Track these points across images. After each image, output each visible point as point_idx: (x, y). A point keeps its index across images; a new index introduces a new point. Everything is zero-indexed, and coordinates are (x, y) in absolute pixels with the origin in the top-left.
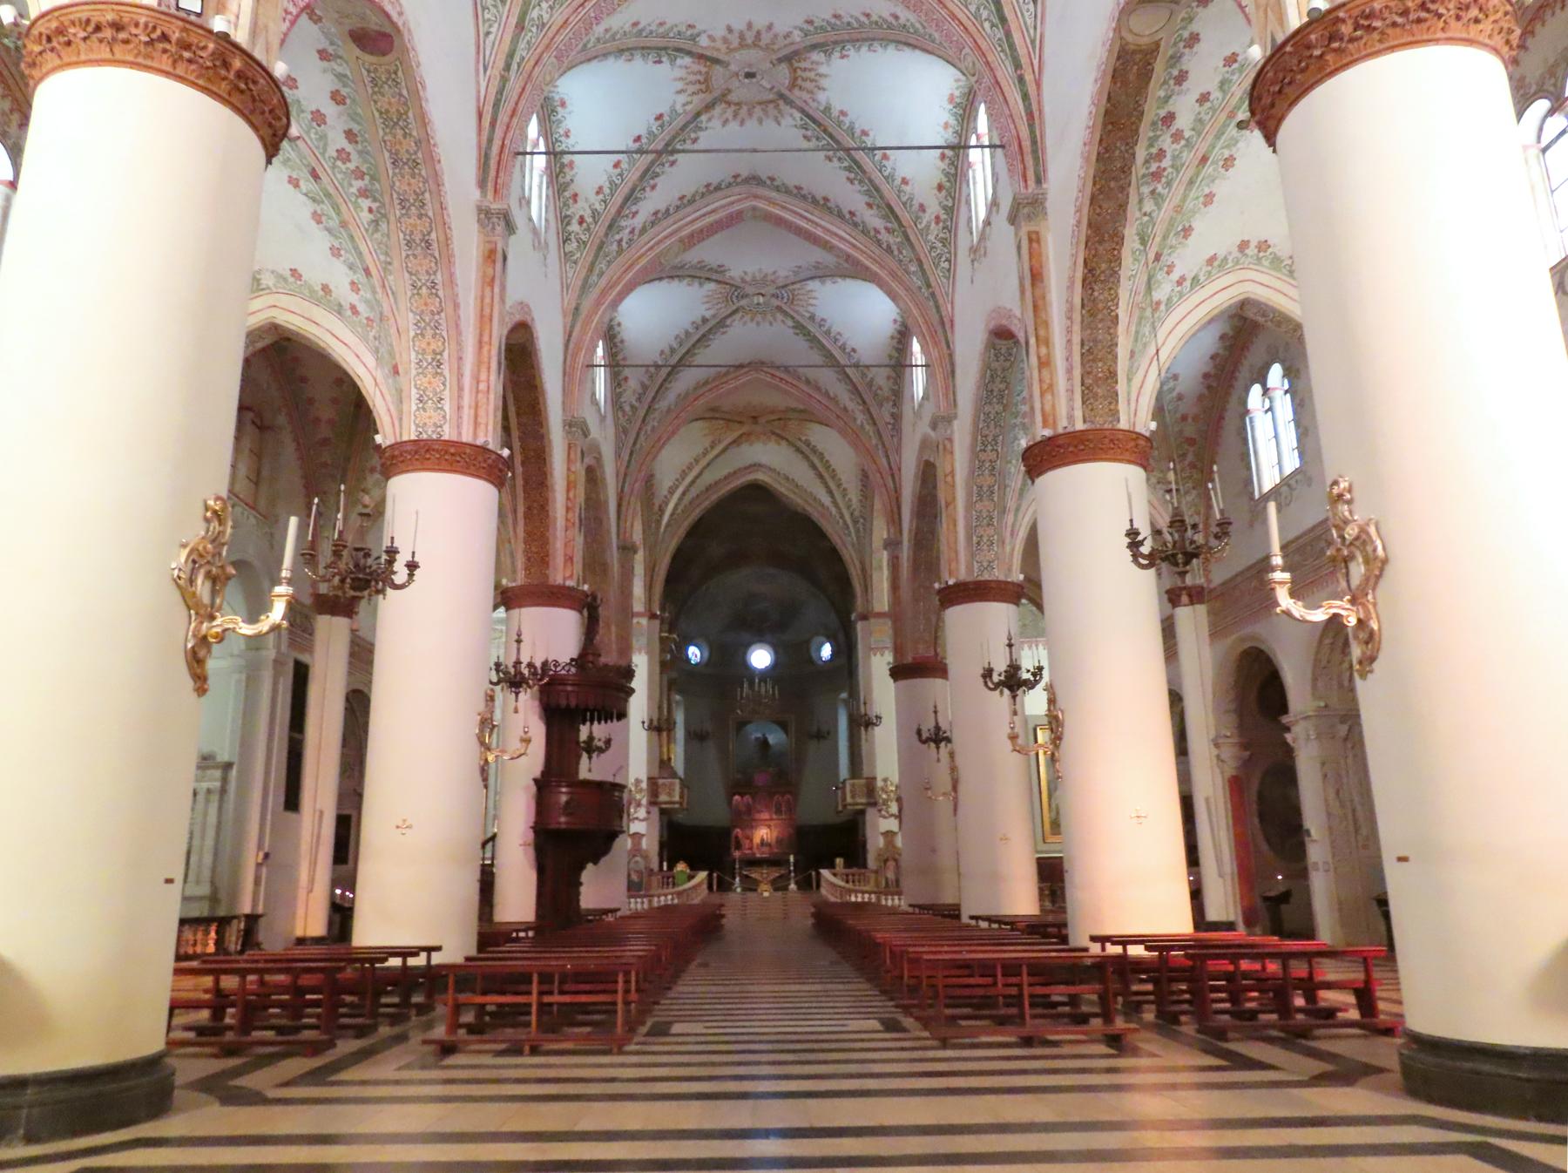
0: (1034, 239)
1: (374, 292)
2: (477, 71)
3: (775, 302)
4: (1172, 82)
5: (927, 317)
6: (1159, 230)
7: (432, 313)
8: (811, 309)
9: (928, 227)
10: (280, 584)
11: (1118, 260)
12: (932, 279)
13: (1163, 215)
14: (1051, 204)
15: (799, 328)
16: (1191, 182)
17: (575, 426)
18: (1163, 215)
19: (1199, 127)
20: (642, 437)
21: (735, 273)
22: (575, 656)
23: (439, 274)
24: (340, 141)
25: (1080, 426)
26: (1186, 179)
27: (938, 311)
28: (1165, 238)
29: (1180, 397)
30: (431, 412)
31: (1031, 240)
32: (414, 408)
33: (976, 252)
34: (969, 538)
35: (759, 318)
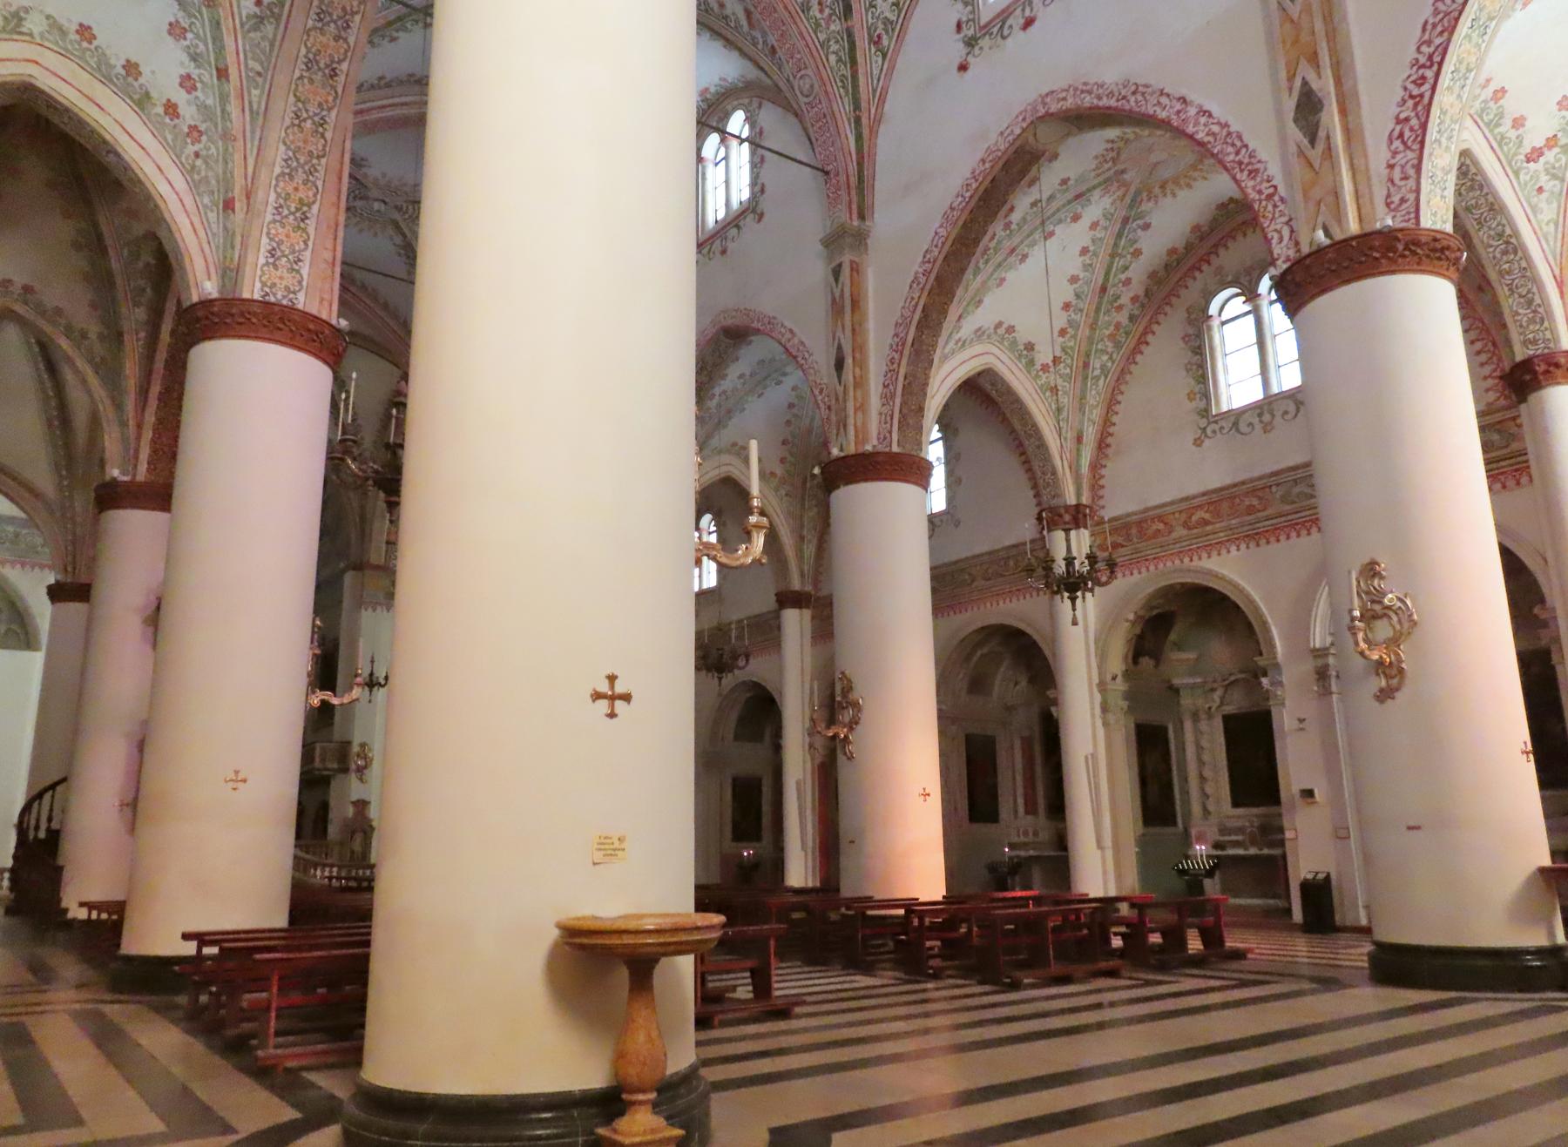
1: (224, 99)
7: (310, 153)
10: (752, 514)
16: (1000, 265)
23: (334, 113)
30: (282, 272)
32: (262, 261)
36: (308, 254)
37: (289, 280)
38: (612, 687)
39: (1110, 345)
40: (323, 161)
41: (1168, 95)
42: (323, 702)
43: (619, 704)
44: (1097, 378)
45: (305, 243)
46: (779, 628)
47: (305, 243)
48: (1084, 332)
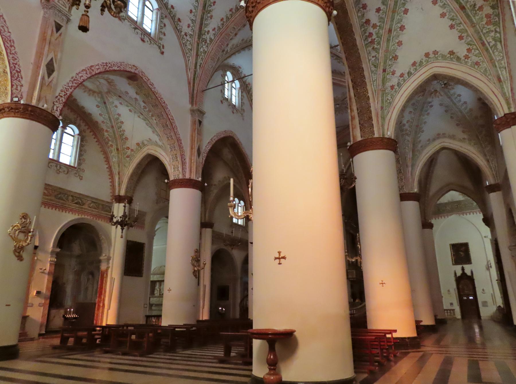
2: (187, 72)
4: (361, 9)
6: (381, 61)
11: (364, 76)
13: (381, 55)
18: (381, 55)
19: (382, 20)
24: (143, 104)
26: (386, 39)
28: (385, 62)
29: (471, 110)
30: (176, 171)
38: (279, 255)
39: (492, 27)
41: (79, 73)
43: (282, 260)
44: (495, 45)
46: (212, 237)
48: (471, 31)
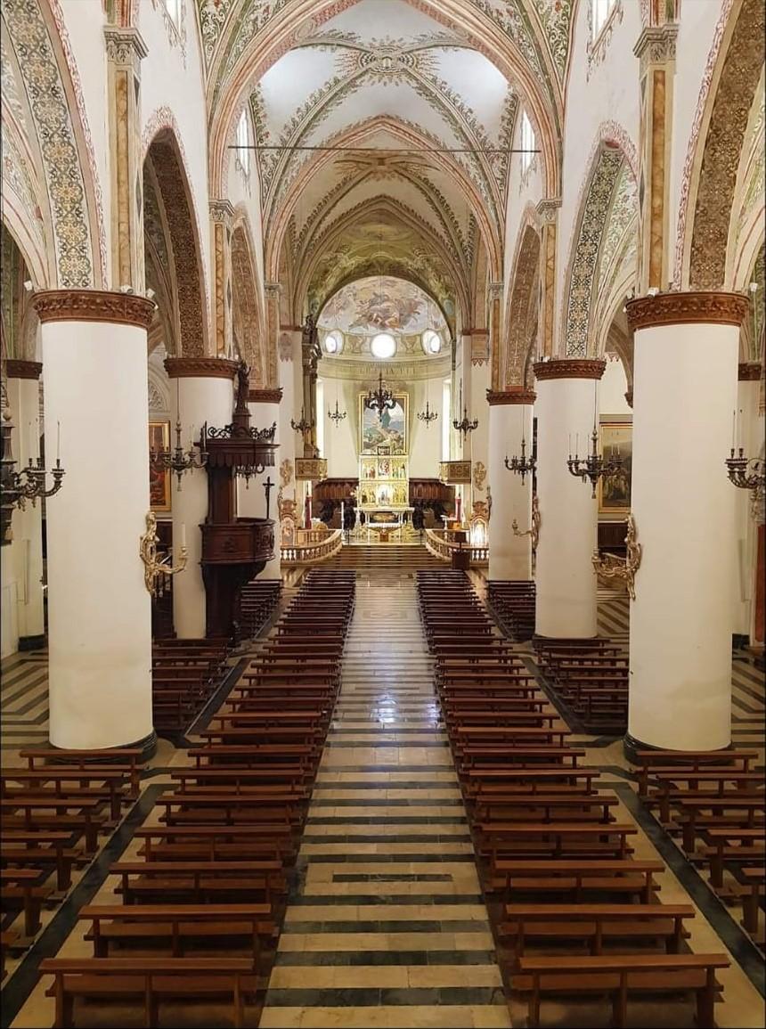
0: (660, 79)
3: (403, 66)
5: (543, 94)
8: (433, 72)
9: (548, 13)
12: (548, 65)
14: (681, 43)
15: (423, 90)
17: (218, 207)
20: (283, 187)
21: (365, 40)
22: (229, 422)
25: (686, 288)
27: (552, 96)
31: (656, 81)
33: (596, 50)
34: (565, 321)
35: (386, 79)
36: (88, 240)
37: (81, 266)
40: (77, 163)
42: (615, 665)
45: (84, 232)
47: (84, 232)
